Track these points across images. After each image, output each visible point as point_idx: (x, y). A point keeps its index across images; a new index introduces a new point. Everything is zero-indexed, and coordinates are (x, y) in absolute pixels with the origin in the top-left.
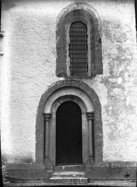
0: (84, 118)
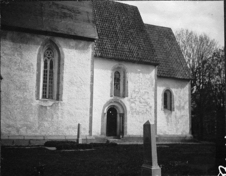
0: (118, 116)
